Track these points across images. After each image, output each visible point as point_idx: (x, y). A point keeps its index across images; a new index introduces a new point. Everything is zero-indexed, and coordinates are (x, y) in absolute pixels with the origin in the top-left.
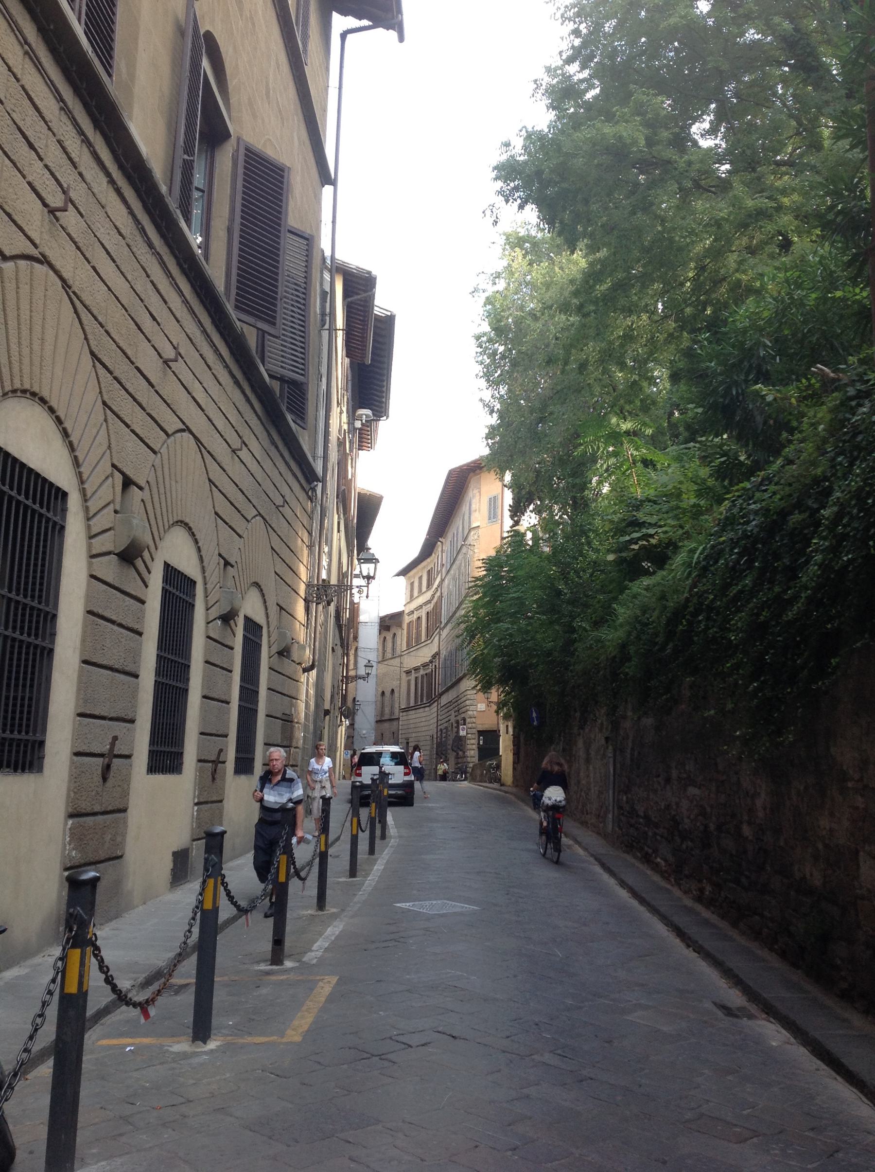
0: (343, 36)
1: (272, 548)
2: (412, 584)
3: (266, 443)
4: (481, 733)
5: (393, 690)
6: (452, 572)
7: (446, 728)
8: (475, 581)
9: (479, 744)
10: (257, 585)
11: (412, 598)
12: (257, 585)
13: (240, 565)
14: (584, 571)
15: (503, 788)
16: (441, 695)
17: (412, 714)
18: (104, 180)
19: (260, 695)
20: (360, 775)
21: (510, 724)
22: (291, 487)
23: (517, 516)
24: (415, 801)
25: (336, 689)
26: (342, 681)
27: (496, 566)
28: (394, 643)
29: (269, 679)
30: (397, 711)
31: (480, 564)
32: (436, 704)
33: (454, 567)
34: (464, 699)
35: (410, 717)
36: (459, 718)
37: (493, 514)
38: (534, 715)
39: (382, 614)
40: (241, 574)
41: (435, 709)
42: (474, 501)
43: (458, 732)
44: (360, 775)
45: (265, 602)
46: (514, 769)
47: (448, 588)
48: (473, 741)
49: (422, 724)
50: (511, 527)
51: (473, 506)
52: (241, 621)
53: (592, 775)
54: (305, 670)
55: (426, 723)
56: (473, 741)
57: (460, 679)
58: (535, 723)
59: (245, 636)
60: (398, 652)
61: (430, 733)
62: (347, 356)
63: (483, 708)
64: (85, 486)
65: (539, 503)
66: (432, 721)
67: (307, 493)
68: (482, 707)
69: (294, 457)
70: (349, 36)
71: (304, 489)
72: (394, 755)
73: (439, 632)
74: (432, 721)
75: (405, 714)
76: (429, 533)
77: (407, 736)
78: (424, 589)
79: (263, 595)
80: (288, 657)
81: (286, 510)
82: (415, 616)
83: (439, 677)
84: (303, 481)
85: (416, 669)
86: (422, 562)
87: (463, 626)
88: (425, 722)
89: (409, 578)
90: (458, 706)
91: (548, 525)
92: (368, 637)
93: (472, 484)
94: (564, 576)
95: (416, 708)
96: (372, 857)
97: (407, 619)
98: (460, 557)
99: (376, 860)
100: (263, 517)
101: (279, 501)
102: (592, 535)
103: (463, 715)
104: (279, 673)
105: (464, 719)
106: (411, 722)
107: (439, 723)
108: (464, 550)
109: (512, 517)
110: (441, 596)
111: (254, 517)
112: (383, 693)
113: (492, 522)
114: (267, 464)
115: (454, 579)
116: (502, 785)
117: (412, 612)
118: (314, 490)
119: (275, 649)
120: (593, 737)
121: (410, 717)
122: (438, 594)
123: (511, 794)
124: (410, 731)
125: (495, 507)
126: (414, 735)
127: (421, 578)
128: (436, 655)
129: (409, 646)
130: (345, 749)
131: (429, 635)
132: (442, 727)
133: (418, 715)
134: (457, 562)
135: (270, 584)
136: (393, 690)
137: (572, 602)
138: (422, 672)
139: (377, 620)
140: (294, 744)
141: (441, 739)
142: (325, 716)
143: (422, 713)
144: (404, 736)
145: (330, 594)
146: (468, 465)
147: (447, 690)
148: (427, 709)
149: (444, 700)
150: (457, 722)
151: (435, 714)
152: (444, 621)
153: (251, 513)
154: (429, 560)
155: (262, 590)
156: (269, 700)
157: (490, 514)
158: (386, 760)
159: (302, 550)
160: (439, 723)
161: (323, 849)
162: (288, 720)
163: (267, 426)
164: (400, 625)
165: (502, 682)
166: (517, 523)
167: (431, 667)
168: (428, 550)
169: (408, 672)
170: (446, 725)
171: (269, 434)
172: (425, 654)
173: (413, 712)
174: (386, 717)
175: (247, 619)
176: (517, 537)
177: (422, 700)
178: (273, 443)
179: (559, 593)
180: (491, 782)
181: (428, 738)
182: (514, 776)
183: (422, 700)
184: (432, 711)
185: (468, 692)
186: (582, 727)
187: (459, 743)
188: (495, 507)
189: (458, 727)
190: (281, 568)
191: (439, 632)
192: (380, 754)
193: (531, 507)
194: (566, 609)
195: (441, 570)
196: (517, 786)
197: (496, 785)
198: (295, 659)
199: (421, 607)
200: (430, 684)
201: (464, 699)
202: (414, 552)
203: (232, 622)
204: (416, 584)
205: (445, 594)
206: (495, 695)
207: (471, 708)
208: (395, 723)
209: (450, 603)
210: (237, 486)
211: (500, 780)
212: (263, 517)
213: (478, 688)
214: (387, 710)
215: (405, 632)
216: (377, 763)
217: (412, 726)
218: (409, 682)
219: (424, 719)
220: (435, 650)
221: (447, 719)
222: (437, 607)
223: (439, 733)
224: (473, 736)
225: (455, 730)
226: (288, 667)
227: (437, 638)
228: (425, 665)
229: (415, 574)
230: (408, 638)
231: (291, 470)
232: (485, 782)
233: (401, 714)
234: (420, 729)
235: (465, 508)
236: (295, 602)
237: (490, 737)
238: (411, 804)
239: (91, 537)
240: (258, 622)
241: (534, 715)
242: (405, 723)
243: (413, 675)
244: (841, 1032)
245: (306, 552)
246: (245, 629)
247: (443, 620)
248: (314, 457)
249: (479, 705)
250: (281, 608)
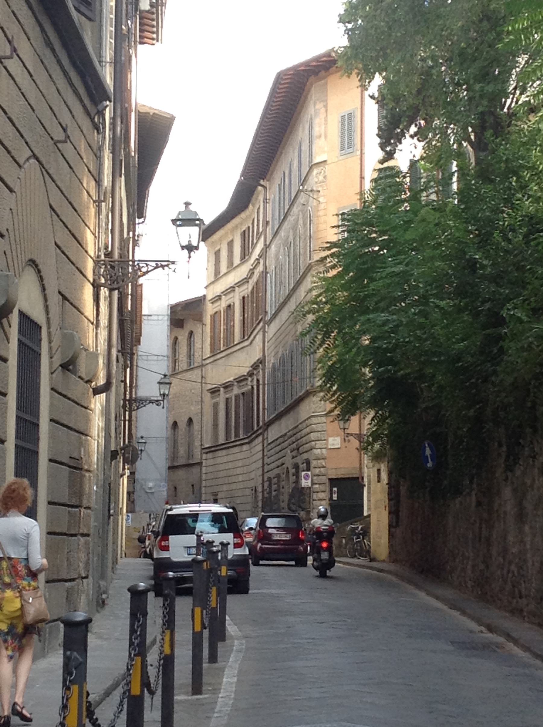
1: (51, 207)
2: (217, 254)
3: (39, 43)
4: (333, 482)
5: (190, 420)
6: (282, 233)
7: (278, 476)
8: (329, 249)
9: (331, 499)
10: (33, 263)
11: (217, 276)
12: (33, 263)
13: (12, 234)
14: (513, 230)
15: (374, 564)
16: (268, 425)
17: (222, 456)
19: (41, 430)
20: (166, 548)
21: (384, 468)
22: (70, 110)
23: (390, 144)
24: (251, 584)
26: (124, 406)
27: (362, 224)
28: (190, 346)
29: (52, 405)
30: (197, 452)
31: (336, 221)
32: (260, 438)
33: (286, 225)
34: (308, 430)
35: (219, 461)
36: (298, 460)
37: (349, 140)
38: (428, 452)
39: (173, 302)
40: (14, 247)
41: (260, 447)
42: (316, 121)
43: (297, 481)
44: (166, 548)
45: (44, 289)
46: (391, 535)
47: (277, 258)
48: (322, 495)
49: (238, 471)
50: (382, 162)
51: (316, 130)
52: (15, 318)
53: (528, 539)
54: (97, 391)
55: (245, 469)
56: (322, 495)
57: (301, 400)
58: (430, 464)
59: (21, 343)
60: (198, 359)
61: (252, 484)
63: (338, 443)
65: (422, 122)
66: (254, 466)
67: (92, 120)
68: (335, 442)
69: (74, 64)
71: (88, 114)
72: (216, 518)
73: (264, 327)
74: (254, 466)
75: (210, 455)
76: (244, 174)
77: (216, 489)
78: (237, 260)
79: (41, 279)
80: (74, 372)
81: (67, 148)
82: (223, 304)
83: (264, 398)
84: (87, 101)
85: (227, 386)
86: (233, 218)
87: (311, 318)
88: (245, 466)
90: (297, 444)
91: (438, 157)
92: (155, 337)
93: (314, 94)
94: (484, 240)
95: (226, 446)
96: (216, 665)
97: (210, 309)
98: (295, 210)
99: (222, 670)
100: (37, 159)
101: (59, 135)
102: (527, 175)
103: (305, 456)
104: (65, 396)
105: (308, 462)
106: (221, 467)
107: (266, 468)
108: (302, 199)
109: (382, 146)
110: (265, 273)
111: (28, 160)
112: (175, 424)
113: (349, 155)
114: (41, 77)
115: (286, 244)
116: (371, 560)
117: (219, 298)
118: (101, 114)
119: (57, 361)
120: (529, 482)
121: (219, 461)
122: (261, 268)
123: (389, 572)
124: (220, 481)
125: (350, 130)
126: (225, 488)
127: (231, 244)
129: (214, 350)
130: (127, 512)
131: (246, 334)
132: (272, 474)
133: (231, 458)
134: (291, 219)
135: (49, 262)
136: (190, 420)
137: (496, 279)
138: (236, 391)
139: (166, 311)
140: (85, 503)
141: (270, 493)
142: (112, 460)
143: (238, 454)
144: (210, 490)
145: (120, 274)
146: (306, 64)
147: (279, 417)
148: (245, 447)
149: (273, 433)
150: (296, 466)
151: (260, 455)
152: (270, 310)
153: (23, 154)
154: (243, 215)
155: (39, 271)
156: (52, 436)
157: (342, 142)
158: (204, 526)
159: (88, 208)
160: (266, 468)
161: (167, 651)
162: (76, 466)
163: (40, 18)
164: (199, 318)
165: (374, 403)
166: (389, 156)
167: (251, 383)
168: (242, 199)
169: (214, 392)
170: (276, 471)
171: (43, 30)
172: (239, 364)
173: (224, 452)
174: (182, 461)
175: (22, 314)
176: (387, 177)
177: (237, 435)
178: (49, 44)
179: (473, 265)
180: (354, 556)
181: (248, 492)
182: (391, 546)
183: (237, 435)
184: (254, 451)
185: (314, 420)
186: (509, 468)
187: (301, 496)
188: (350, 130)
189: (297, 475)
190: (63, 238)
191: (264, 327)
192: (195, 516)
193: (413, 129)
194: (486, 289)
195: (265, 230)
196: (395, 561)
197: (361, 561)
198: (83, 376)
199: (232, 289)
200: (249, 409)
201: (308, 430)
203: (5, 321)
204: (224, 254)
205: (271, 268)
206: (364, 422)
207: (319, 444)
208: (195, 470)
209: (279, 283)
210: (5, 113)
211: (369, 552)
212: (37, 159)
213: (336, 412)
214: (182, 451)
215: (208, 329)
216: (192, 531)
217: (222, 474)
218: (216, 406)
219: (240, 464)
220: (257, 355)
221: (279, 463)
222: (259, 289)
223: (266, 484)
224: (322, 488)
225: (292, 478)
226: (76, 388)
227: (259, 337)
228: (241, 380)
230: (213, 338)
231: (72, 85)
232: (346, 556)
233: (204, 456)
234: (233, 479)
235: (302, 133)
236: (82, 287)
237: (348, 489)
238: (247, 592)
240: (36, 320)
241: (428, 452)
242: (210, 469)
243: (222, 396)
245: (93, 210)
246: (20, 332)
247: (268, 309)
248: (100, 62)
249: (331, 440)
250: (65, 298)
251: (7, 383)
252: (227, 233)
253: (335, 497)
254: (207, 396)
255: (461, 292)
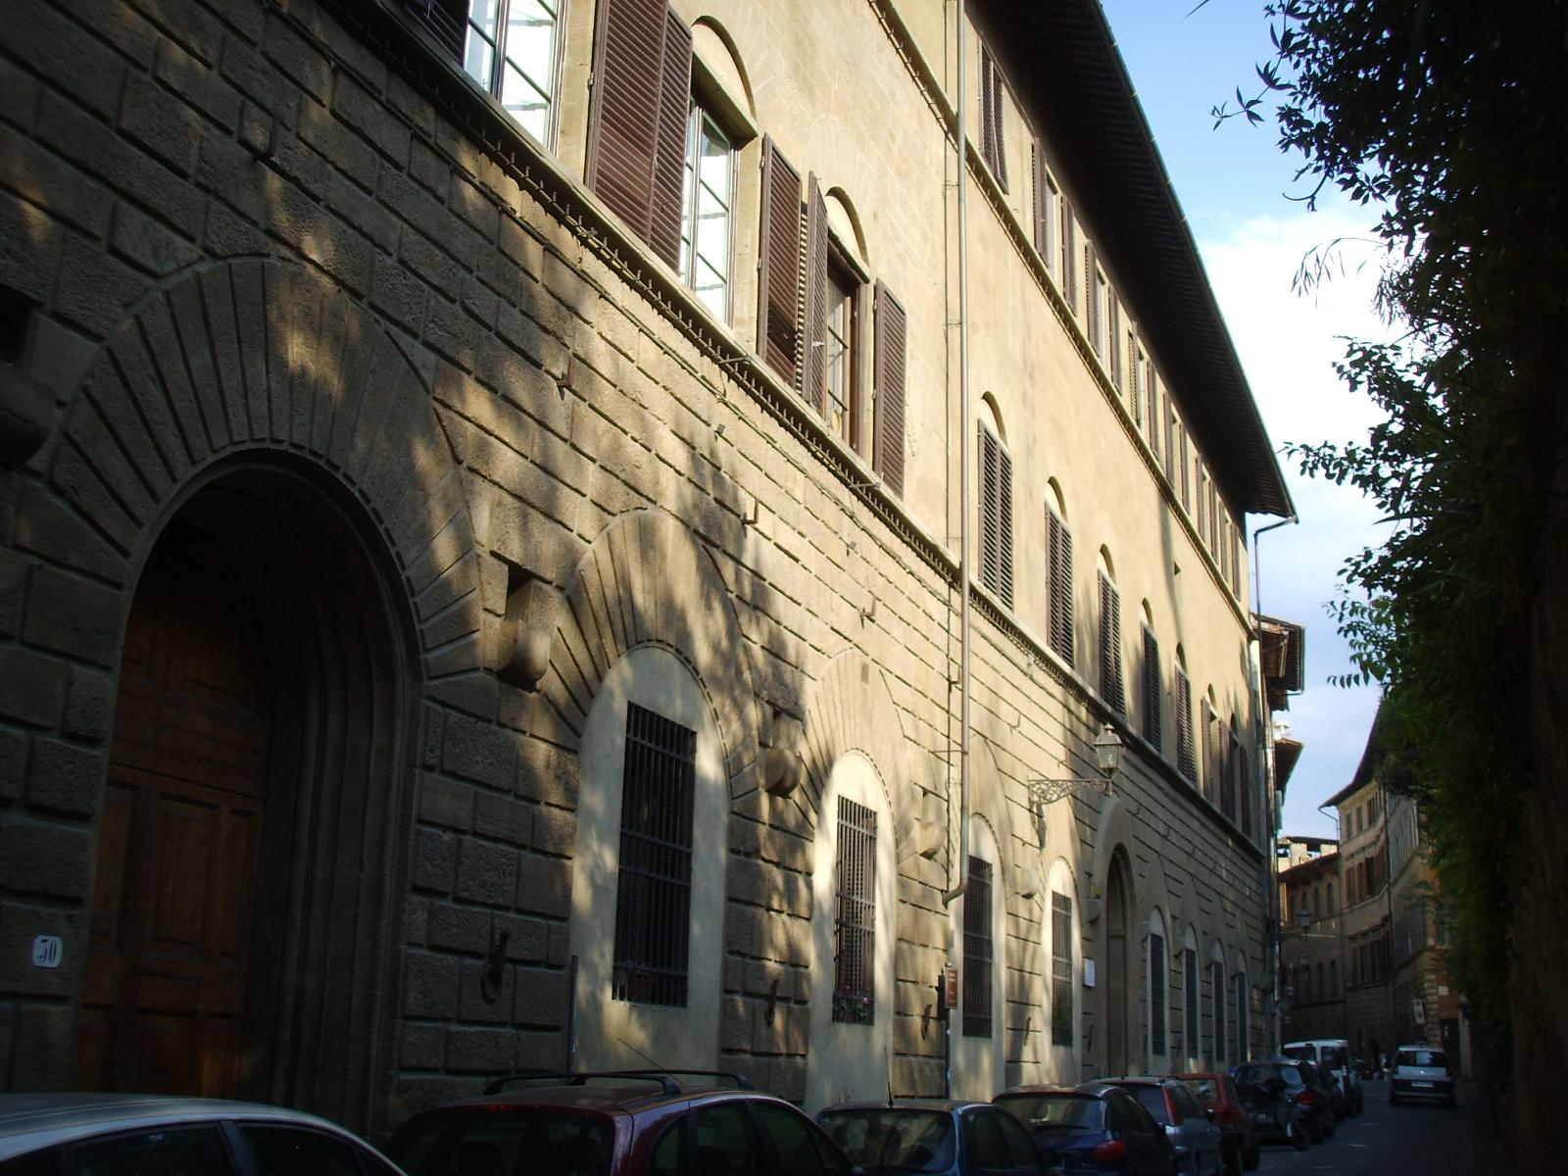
2: (1348, 817)
5: (1333, 963)
18: (1154, 787)
25: (1237, 884)
64: (408, 135)
70: (1260, 535)
78: (1365, 826)
85: (1364, 934)
89: (1344, 808)
97: (1345, 865)
101: (1189, 849)
127: (1359, 810)
128: (1387, 919)
136: (1333, 963)
164: (1336, 872)
167: (1382, 934)
169: (1352, 938)
202: (1348, 778)
215: (1344, 881)
227: (1386, 896)
251: (567, 940)
252: (1355, 801)
253: (1446, 1034)
254: (1347, 942)
255: (1303, 142)
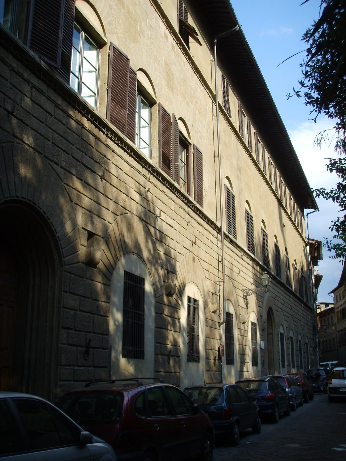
0: (307, 215)
2: (337, 296)
62: (289, 415)
86: (340, 288)
117: (338, 307)
127: (340, 294)
164: (334, 312)
169: (339, 331)
202: (336, 285)
215: (336, 315)
229: (337, 293)
239: (156, 298)
244: (189, 31)
246: (251, 325)
